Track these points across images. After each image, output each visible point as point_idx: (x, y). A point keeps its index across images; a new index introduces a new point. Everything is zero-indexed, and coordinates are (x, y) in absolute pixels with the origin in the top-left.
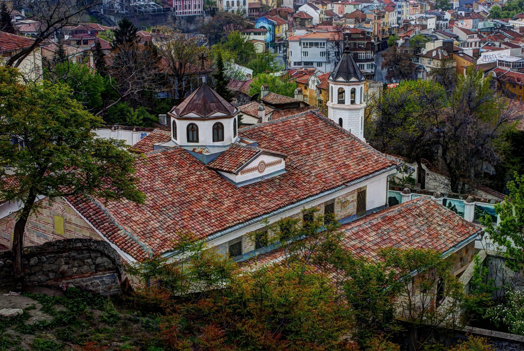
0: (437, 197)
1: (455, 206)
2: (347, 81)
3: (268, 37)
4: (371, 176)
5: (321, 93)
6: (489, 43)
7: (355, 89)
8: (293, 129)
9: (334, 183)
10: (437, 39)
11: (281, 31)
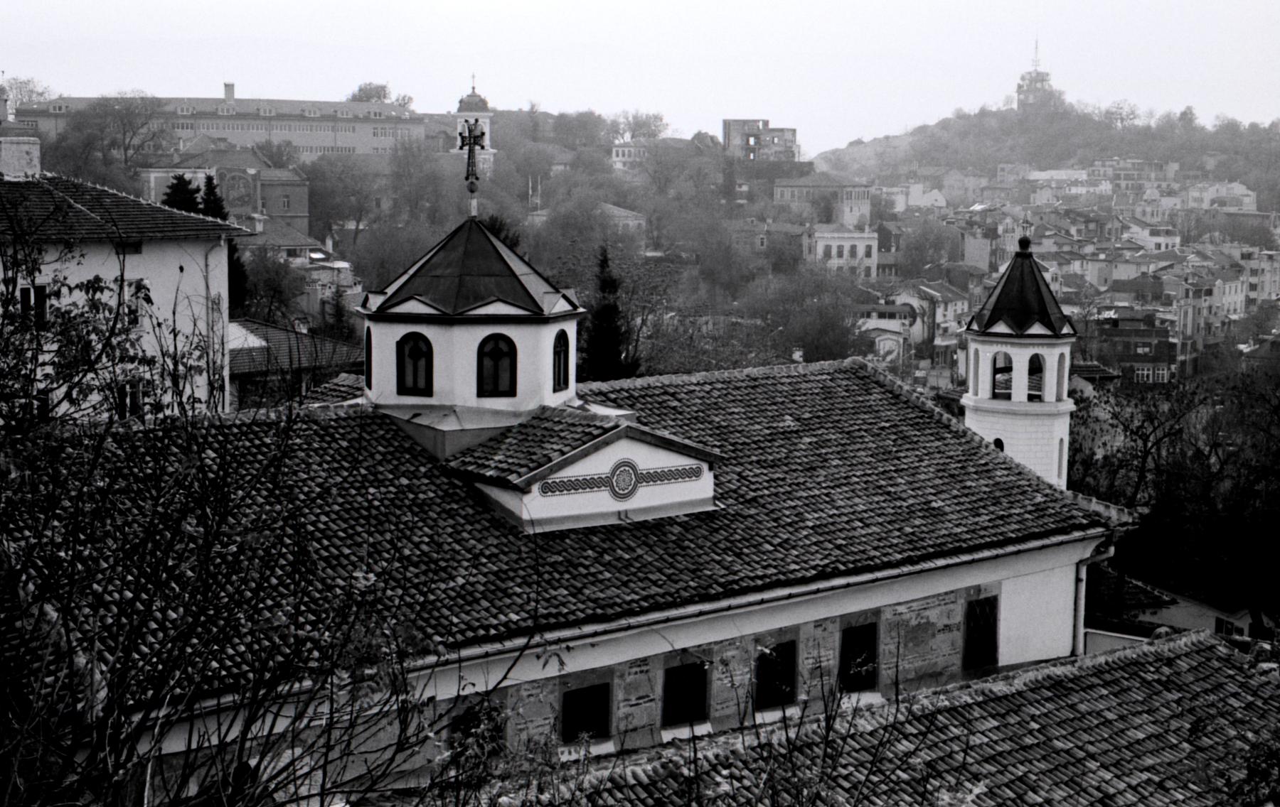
2: (1019, 333)
3: (918, 331)
4: (1011, 549)
9: (873, 553)
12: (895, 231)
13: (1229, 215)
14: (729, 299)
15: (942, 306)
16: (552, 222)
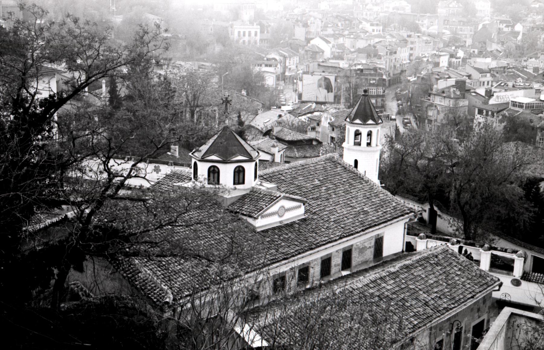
0: (453, 244)
1: (471, 253)
3: (279, 70)
4: (389, 223)
5: (333, 130)
6: (502, 83)
7: (371, 132)
8: (312, 173)
9: (352, 229)
10: (450, 77)
11: (292, 62)
12: (266, 24)
13: (400, 14)
14: (199, 54)
15: (289, 59)
16: (124, 22)
